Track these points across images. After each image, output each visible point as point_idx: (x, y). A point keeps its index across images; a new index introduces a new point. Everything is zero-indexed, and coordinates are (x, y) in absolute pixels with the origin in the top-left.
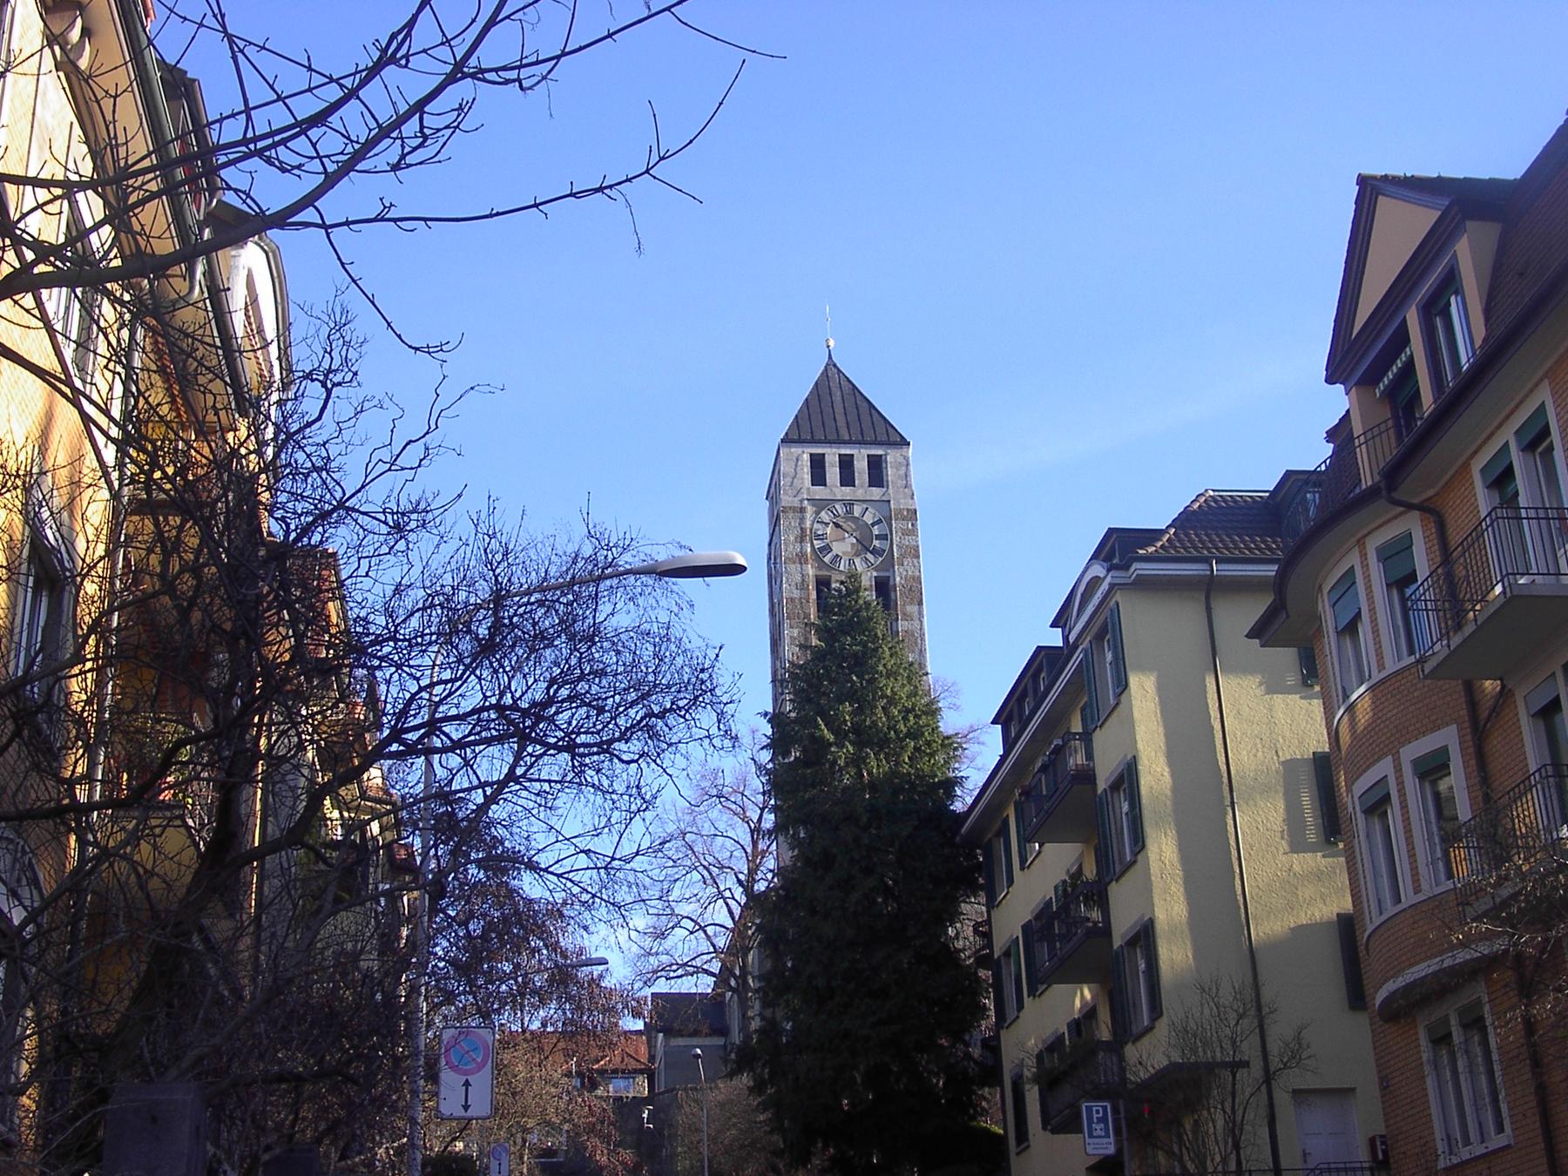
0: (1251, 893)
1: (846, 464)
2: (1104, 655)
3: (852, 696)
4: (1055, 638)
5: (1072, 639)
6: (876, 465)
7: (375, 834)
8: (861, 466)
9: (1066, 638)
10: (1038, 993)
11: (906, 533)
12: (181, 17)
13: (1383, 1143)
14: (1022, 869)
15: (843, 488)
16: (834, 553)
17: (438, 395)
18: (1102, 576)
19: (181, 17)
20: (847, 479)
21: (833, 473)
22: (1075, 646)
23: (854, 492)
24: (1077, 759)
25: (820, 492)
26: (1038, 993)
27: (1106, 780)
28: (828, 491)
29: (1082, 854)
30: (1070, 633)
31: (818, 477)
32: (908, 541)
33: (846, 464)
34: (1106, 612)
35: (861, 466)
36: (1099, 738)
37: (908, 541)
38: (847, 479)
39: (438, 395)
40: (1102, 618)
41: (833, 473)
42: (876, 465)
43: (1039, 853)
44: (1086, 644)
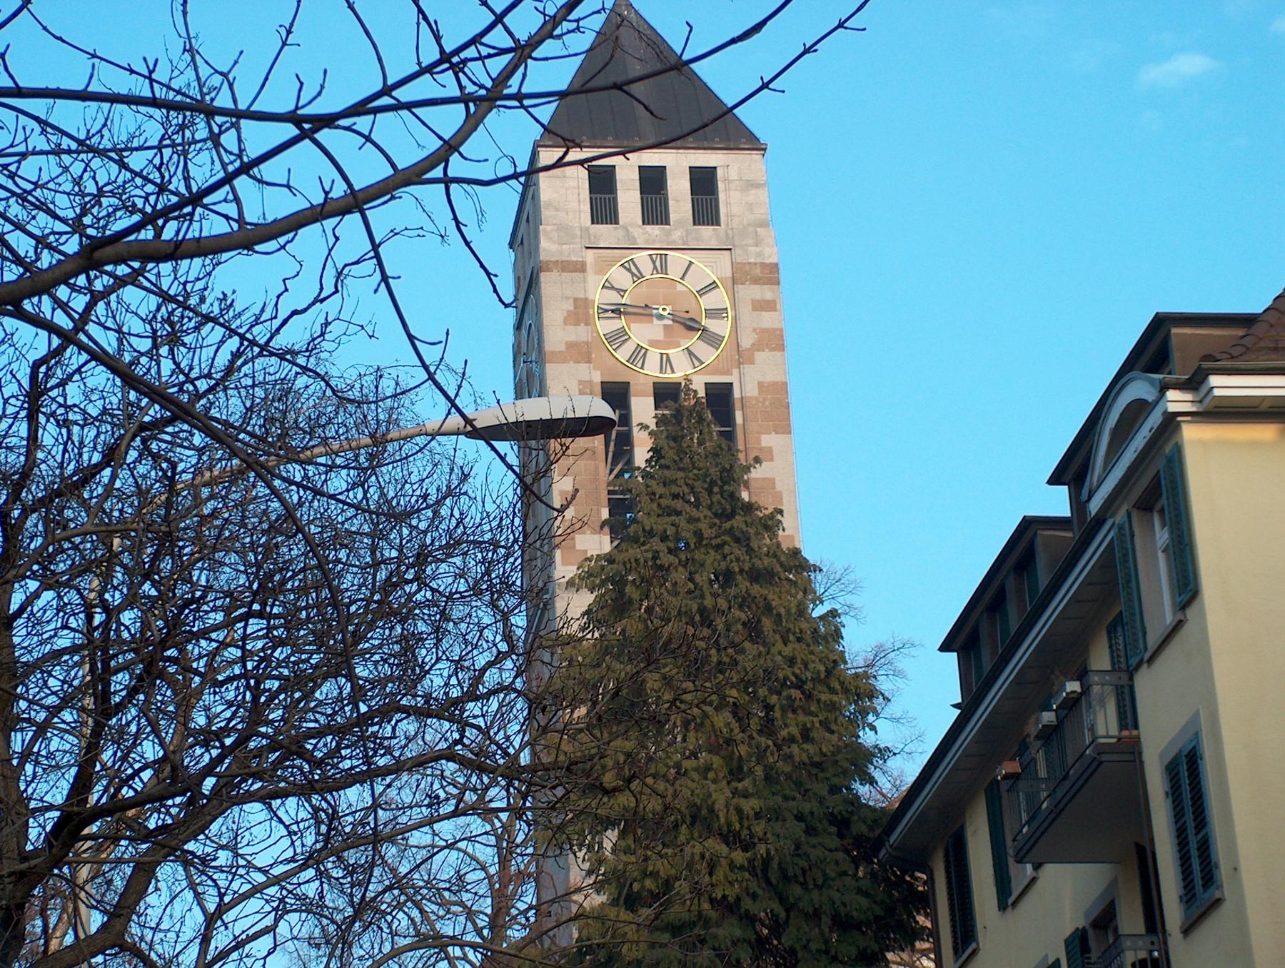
0: (661, 242)
1: (653, 181)
2: (1154, 534)
3: (315, 683)
4: (1057, 503)
5: (1095, 506)
6: (703, 182)
7: (569, 615)
8: (679, 189)
9: (1078, 503)
10: (1010, 901)
11: (769, 306)
12: (292, 24)
13: (1127, 724)
14: (1003, 906)
15: (648, 228)
16: (635, 340)
17: (337, 239)
18: (1150, 398)
19: (292, 24)
20: (655, 210)
21: (629, 197)
22: (1099, 521)
23: (668, 234)
24: (1105, 723)
25: (605, 234)
26: (1010, 901)
27: (1161, 755)
28: (620, 233)
29: (1113, 884)
30: (1090, 497)
31: (604, 210)
32: (768, 320)
33: (653, 181)
34: (1160, 464)
35: (679, 189)
36: (1146, 684)
37: (768, 320)
38: (655, 210)
39: (337, 239)
40: (1150, 473)
41: (629, 197)
42: (703, 182)
43: (1034, 880)
44: (1120, 517)
